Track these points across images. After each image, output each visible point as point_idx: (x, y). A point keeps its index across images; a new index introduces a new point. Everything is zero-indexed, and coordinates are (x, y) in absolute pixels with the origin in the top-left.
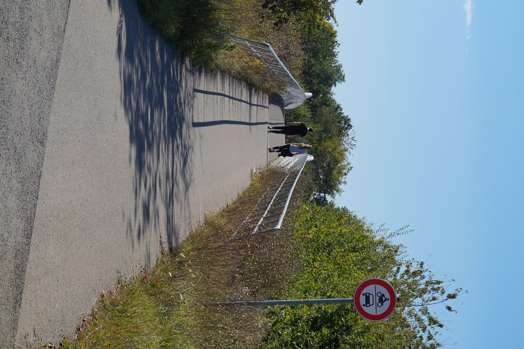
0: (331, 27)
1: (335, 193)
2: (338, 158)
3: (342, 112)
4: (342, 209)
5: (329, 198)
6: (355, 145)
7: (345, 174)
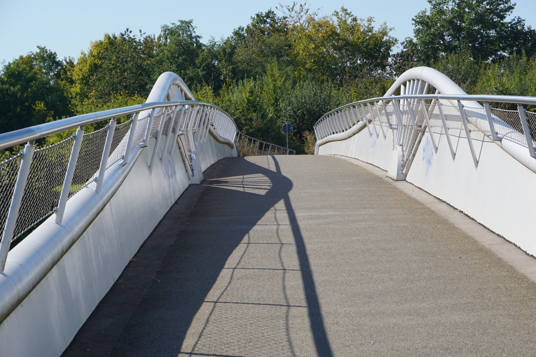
0: (98, 45)
1: (387, 38)
2: (327, 32)
3: (245, 28)
4: (416, 26)
5: (396, 50)
6: (301, 6)
7: (355, 20)
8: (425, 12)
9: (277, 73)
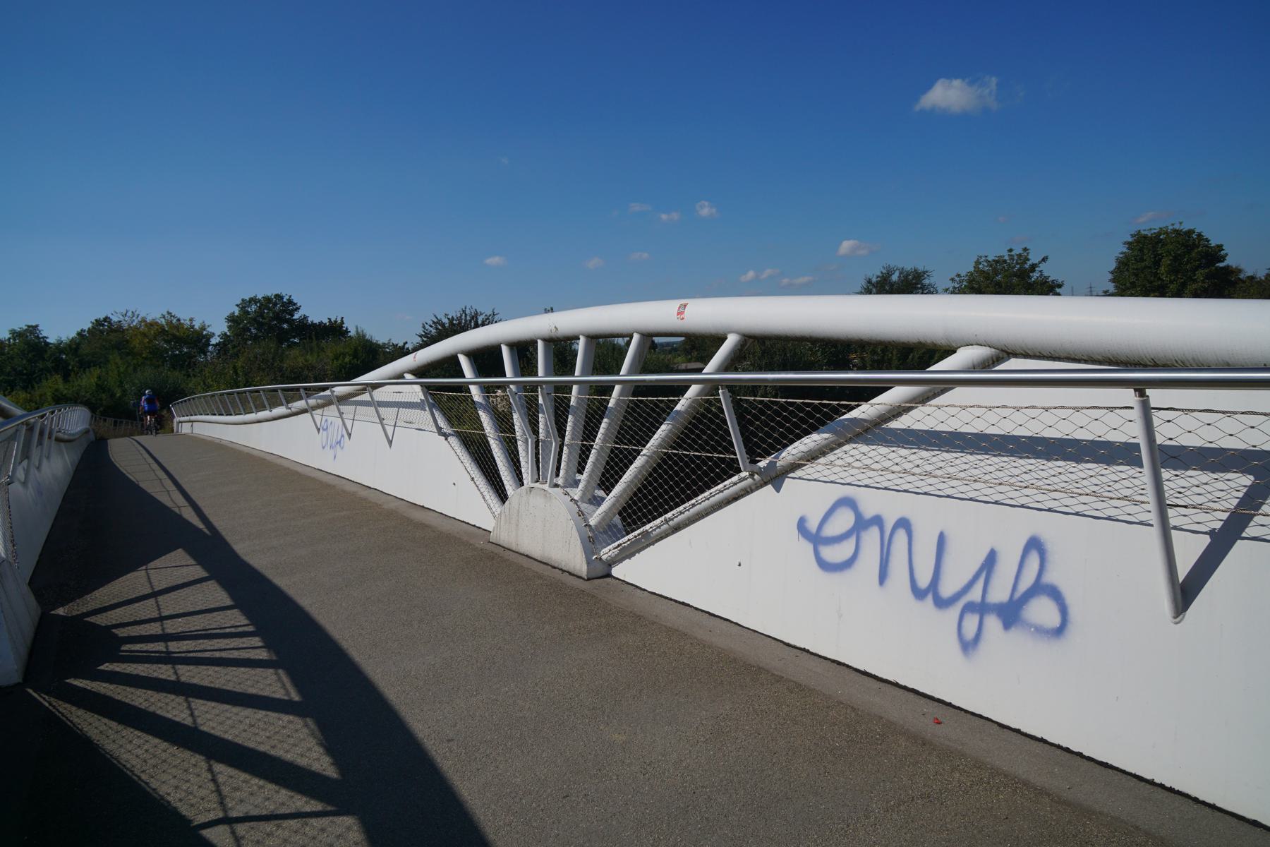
3: (87, 330)
5: (214, 341)
7: (179, 320)
8: (234, 313)
9: (118, 360)
